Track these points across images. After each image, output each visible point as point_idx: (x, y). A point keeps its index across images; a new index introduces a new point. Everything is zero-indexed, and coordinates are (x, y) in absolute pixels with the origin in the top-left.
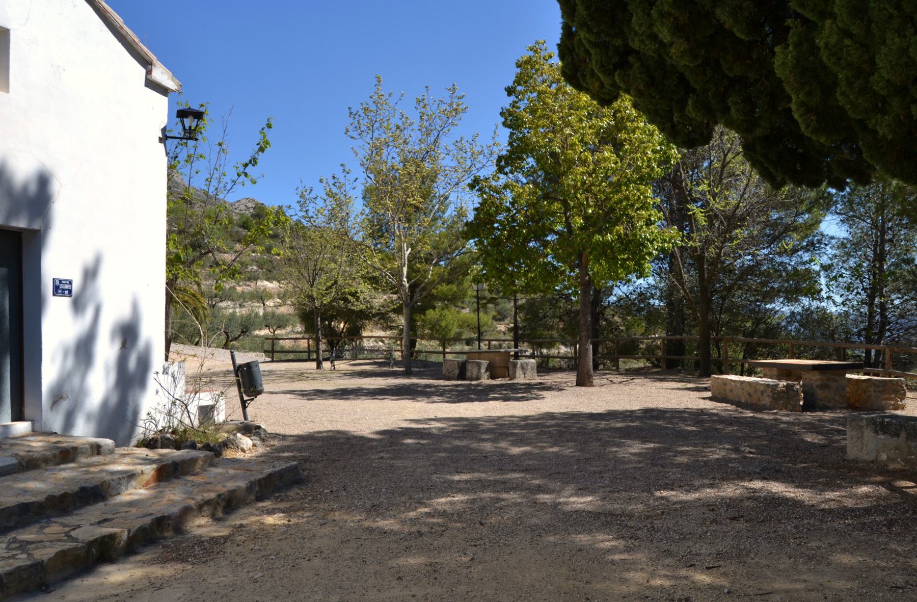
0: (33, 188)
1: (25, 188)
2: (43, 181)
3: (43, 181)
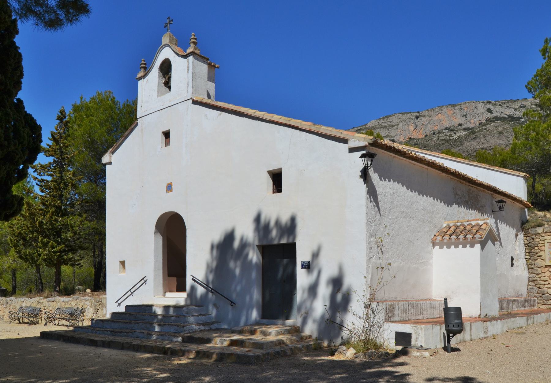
0: (289, 223)
1: (286, 224)
2: (293, 220)
3: (293, 220)
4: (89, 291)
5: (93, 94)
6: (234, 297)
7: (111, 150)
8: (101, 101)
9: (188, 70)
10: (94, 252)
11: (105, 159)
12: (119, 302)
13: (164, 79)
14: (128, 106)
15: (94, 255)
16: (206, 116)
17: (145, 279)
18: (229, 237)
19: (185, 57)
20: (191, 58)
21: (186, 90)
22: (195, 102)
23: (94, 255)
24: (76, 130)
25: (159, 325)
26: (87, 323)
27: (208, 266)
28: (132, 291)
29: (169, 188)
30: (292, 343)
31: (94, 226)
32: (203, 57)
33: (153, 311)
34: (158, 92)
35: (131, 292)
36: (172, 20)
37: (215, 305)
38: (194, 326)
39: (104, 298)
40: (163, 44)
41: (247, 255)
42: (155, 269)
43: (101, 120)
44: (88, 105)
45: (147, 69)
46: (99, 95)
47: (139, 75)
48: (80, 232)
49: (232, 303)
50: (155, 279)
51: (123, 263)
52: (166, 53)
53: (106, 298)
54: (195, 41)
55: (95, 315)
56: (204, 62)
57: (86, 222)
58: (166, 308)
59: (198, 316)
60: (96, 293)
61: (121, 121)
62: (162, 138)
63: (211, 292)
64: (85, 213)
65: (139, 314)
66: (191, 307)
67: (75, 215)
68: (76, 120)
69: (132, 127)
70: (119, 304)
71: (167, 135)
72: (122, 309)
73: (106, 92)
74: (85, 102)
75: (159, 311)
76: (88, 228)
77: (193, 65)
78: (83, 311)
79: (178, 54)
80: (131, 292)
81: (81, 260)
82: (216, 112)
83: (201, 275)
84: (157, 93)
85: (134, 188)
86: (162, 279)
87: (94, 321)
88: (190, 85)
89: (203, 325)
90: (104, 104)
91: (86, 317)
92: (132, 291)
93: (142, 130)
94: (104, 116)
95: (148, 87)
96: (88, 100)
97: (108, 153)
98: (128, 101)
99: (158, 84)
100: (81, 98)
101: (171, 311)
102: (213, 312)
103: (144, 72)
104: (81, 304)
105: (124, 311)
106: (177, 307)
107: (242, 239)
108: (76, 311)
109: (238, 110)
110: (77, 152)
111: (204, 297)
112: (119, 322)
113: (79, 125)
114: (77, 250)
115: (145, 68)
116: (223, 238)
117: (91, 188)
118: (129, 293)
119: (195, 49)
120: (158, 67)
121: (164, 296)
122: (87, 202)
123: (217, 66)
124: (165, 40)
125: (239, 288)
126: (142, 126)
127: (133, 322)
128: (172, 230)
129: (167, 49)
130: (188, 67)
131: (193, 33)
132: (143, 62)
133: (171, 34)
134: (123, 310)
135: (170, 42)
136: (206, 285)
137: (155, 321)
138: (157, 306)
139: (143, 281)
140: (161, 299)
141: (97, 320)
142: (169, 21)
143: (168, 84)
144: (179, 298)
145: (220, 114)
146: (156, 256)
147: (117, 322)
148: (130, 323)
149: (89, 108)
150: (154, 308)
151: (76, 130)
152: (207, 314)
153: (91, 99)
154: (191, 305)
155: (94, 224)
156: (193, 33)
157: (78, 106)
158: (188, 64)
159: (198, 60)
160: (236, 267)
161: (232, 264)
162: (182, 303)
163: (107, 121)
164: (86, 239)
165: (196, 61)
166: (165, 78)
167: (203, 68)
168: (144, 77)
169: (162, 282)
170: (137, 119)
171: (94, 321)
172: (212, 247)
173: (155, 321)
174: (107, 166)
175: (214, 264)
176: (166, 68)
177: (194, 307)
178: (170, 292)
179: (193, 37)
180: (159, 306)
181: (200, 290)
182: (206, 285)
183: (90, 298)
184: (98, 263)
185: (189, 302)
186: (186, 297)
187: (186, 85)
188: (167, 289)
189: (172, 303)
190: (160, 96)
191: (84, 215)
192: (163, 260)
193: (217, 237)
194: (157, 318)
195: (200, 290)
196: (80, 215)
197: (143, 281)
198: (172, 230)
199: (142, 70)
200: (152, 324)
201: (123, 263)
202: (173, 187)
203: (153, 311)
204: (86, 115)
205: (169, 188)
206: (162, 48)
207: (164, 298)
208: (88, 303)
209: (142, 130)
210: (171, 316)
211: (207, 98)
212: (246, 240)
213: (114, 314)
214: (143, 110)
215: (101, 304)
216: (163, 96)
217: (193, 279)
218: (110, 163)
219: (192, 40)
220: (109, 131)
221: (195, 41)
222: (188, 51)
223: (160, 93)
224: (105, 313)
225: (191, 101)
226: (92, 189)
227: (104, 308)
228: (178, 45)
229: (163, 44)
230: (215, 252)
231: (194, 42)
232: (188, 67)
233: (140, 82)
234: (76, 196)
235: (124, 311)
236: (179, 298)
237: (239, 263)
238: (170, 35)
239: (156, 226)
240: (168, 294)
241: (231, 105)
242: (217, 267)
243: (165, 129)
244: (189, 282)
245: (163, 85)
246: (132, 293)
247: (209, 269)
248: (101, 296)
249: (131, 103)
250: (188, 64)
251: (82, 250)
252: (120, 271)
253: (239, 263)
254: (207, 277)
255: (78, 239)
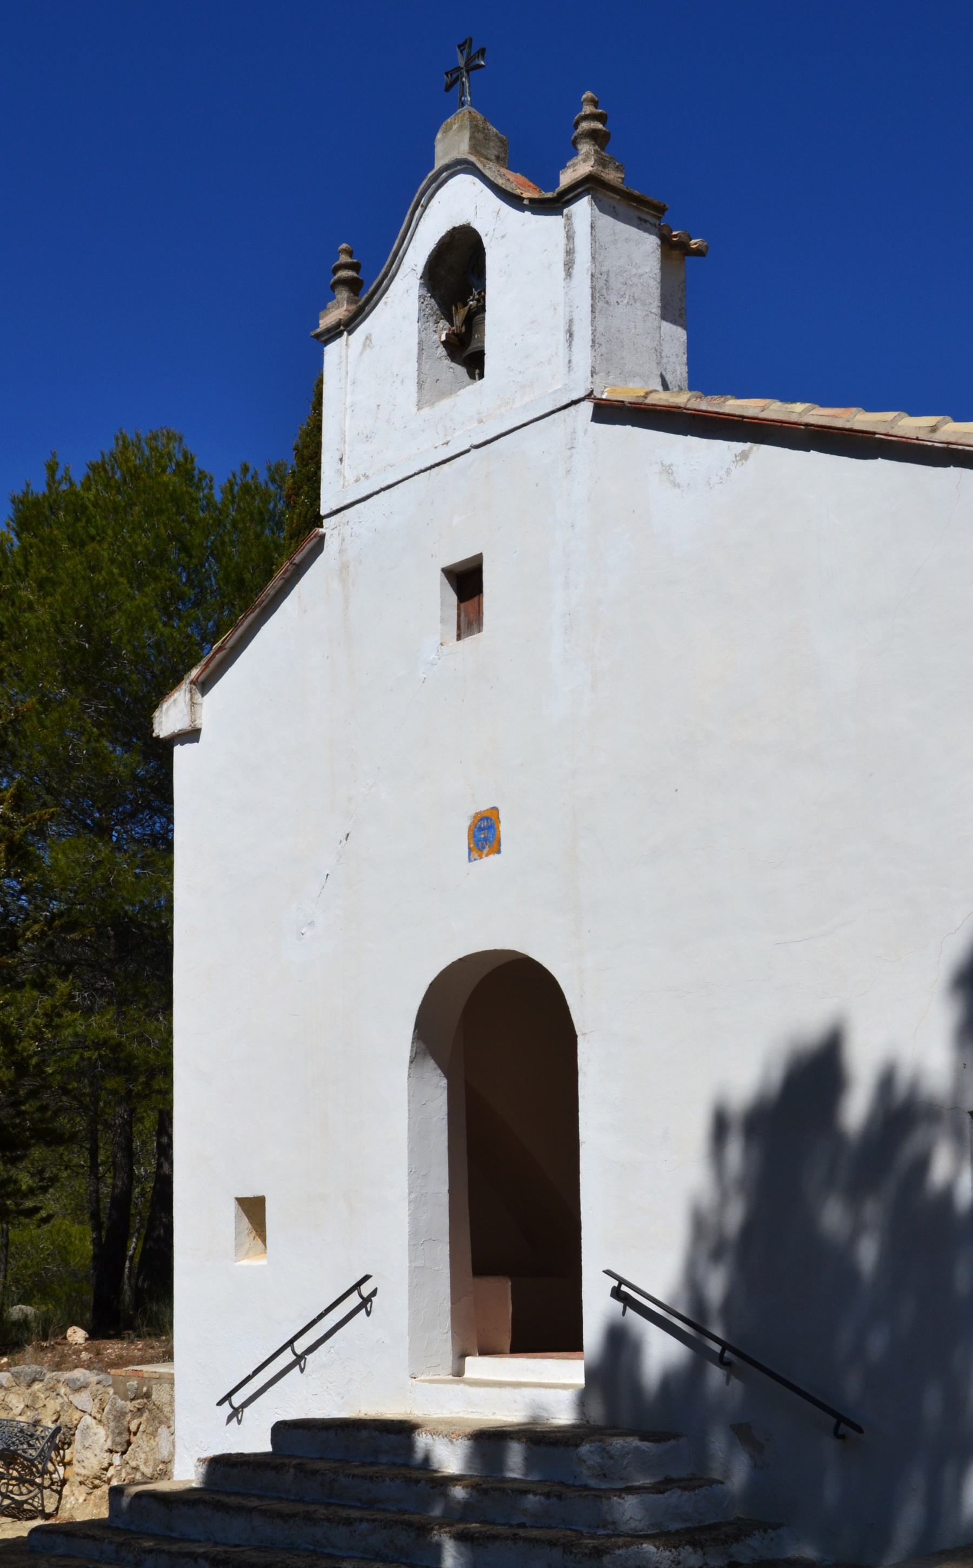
4: (77, 1335)
5: (102, 447)
6: (852, 1387)
7: (194, 673)
8: (134, 474)
9: (569, 266)
10: (94, 1153)
11: (169, 718)
12: (237, 1400)
13: (443, 324)
14: (246, 489)
15: (94, 1165)
16: (668, 470)
17: (366, 1289)
18: (816, 1073)
19: (552, 205)
20: (583, 209)
21: (561, 361)
22: (607, 412)
23: (94, 1165)
24: (31, 607)
25: (461, 1537)
26: (82, 1505)
27: (700, 1226)
28: (300, 1346)
29: (485, 834)
30: (129, 1335)
31: (102, 1035)
32: (640, 202)
33: (419, 1455)
34: (420, 385)
35: (296, 1354)
36: (482, 52)
37: (742, 1433)
38: (648, 1547)
39: (160, 1378)
40: (439, 163)
41: (922, 1165)
42: (417, 1238)
43: (135, 555)
44: (76, 494)
45: (364, 291)
46: (126, 447)
47: (327, 320)
48: (43, 1062)
49: (843, 1425)
50: (415, 1288)
51: (253, 1209)
52: (459, 202)
53: (171, 1380)
54: (599, 126)
55: (117, 1459)
56: (641, 224)
57: (68, 1016)
58: (488, 1442)
59: (659, 1488)
60: (112, 1349)
61: (238, 545)
62: (440, 599)
63: (722, 1362)
64: (63, 976)
65: (339, 1474)
66: (618, 1443)
67: (20, 986)
68: (27, 564)
69: (297, 559)
70: (236, 1413)
71: (466, 581)
72: (253, 1438)
73: (155, 438)
74: (64, 487)
75: (450, 1459)
76: (80, 1042)
77: (594, 239)
78: (61, 1439)
79: (514, 201)
80: (296, 1354)
81: (44, 1190)
82: (722, 450)
83: (660, 1273)
84: (414, 388)
85: (306, 851)
86: (448, 1290)
87: (125, 1501)
88: (583, 333)
89: (694, 1544)
90: (149, 488)
91: (77, 1468)
92: (300, 1346)
93: (344, 567)
94: (145, 540)
95: (373, 375)
96: (78, 478)
97: (185, 686)
98: (246, 469)
99: (421, 350)
100: (52, 469)
101: (515, 1462)
102: (735, 1471)
103: (350, 302)
104: (53, 1405)
105: (267, 1447)
106: (537, 1438)
107: (886, 1082)
108: (28, 1435)
109: (839, 423)
110: (32, 701)
111: (682, 1385)
112: (251, 1510)
113: (41, 584)
114: (27, 1147)
115: (354, 286)
116: (777, 1075)
117: (93, 858)
118: (287, 1357)
119: (601, 162)
120: (420, 269)
121: (459, 1372)
122: (72, 926)
123: (695, 243)
124: (452, 142)
125: (877, 1344)
126: (341, 551)
127: (322, 1511)
128: (501, 1045)
129: (463, 184)
130: (570, 252)
131: (588, 94)
132: (344, 259)
133: (479, 116)
134: (263, 1445)
135: (475, 148)
136: (690, 1323)
137: (437, 1512)
138: (434, 1433)
139: (354, 1300)
140: (477, 1398)
141: (139, 1495)
142: (469, 60)
143: (466, 352)
144: (548, 1388)
145: (744, 456)
146: (416, 1174)
147: (240, 1509)
148: (309, 1518)
149: (84, 508)
150: (422, 1441)
151: (31, 607)
152: (697, 1481)
153: (93, 468)
154: (612, 1428)
155: (102, 1024)
156: (588, 94)
157: (36, 503)
158: (570, 237)
159: (615, 214)
160: (856, 1231)
161: (833, 1216)
162: (563, 1414)
163: (161, 558)
164: (66, 1091)
165: (606, 221)
166: (450, 320)
167: (640, 251)
168: (349, 325)
169: (448, 1304)
170: (318, 520)
171: (125, 1501)
172: (720, 1126)
173: (437, 1512)
174: (178, 750)
175: (735, 1216)
176: (459, 272)
177: (634, 1442)
178: (484, 1352)
179: (588, 109)
180: (447, 1431)
181: (660, 1351)
182: (690, 1323)
183: (91, 1377)
184: (114, 1200)
185: (597, 1413)
186: (581, 1380)
187: (562, 336)
188: (474, 1339)
189: (507, 1411)
190: (431, 403)
191: (63, 987)
192: (451, 1191)
193: (746, 1071)
194: (445, 1495)
195: (660, 1351)
196: (42, 985)
197: (354, 1300)
198: (501, 1045)
199: (343, 295)
200: (424, 1529)
201: (253, 1209)
202: (504, 829)
203: (419, 1455)
204: (70, 539)
205: (485, 834)
206: (439, 181)
207: (459, 1389)
208: (83, 1400)
209: (344, 567)
210: (521, 1490)
211: (660, 388)
212: (914, 1087)
213: (221, 1467)
214: (350, 475)
215: (145, 1411)
216: (445, 403)
217: (617, 1293)
218: (192, 735)
219: (585, 125)
220: (169, 604)
221: (599, 126)
222: (567, 178)
223: (428, 391)
224: (164, 1453)
225: (587, 408)
226: (94, 867)
227: (163, 1430)
228: (510, 161)
229: (439, 163)
230: (735, 1151)
231: (593, 135)
232: (570, 252)
233: (332, 352)
234: (23, 901)
235: (267, 1447)
236: (548, 1388)
237: (873, 1210)
238: (472, 119)
239: (418, 1025)
240: (477, 1366)
241: (799, 407)
242: (749, 1229)
243: (459, 555)
244: (597, 1309)
245: (442, 351)
246: (299, 1359)
247: (705, 1238)
248: (147, 1369)
249: (263, 477)
250: (570, 237)
251: (48, 1144)
252: (238, 1246)
253: (873, 1210)
254: (693, 1284)
255: (33, 1094)
